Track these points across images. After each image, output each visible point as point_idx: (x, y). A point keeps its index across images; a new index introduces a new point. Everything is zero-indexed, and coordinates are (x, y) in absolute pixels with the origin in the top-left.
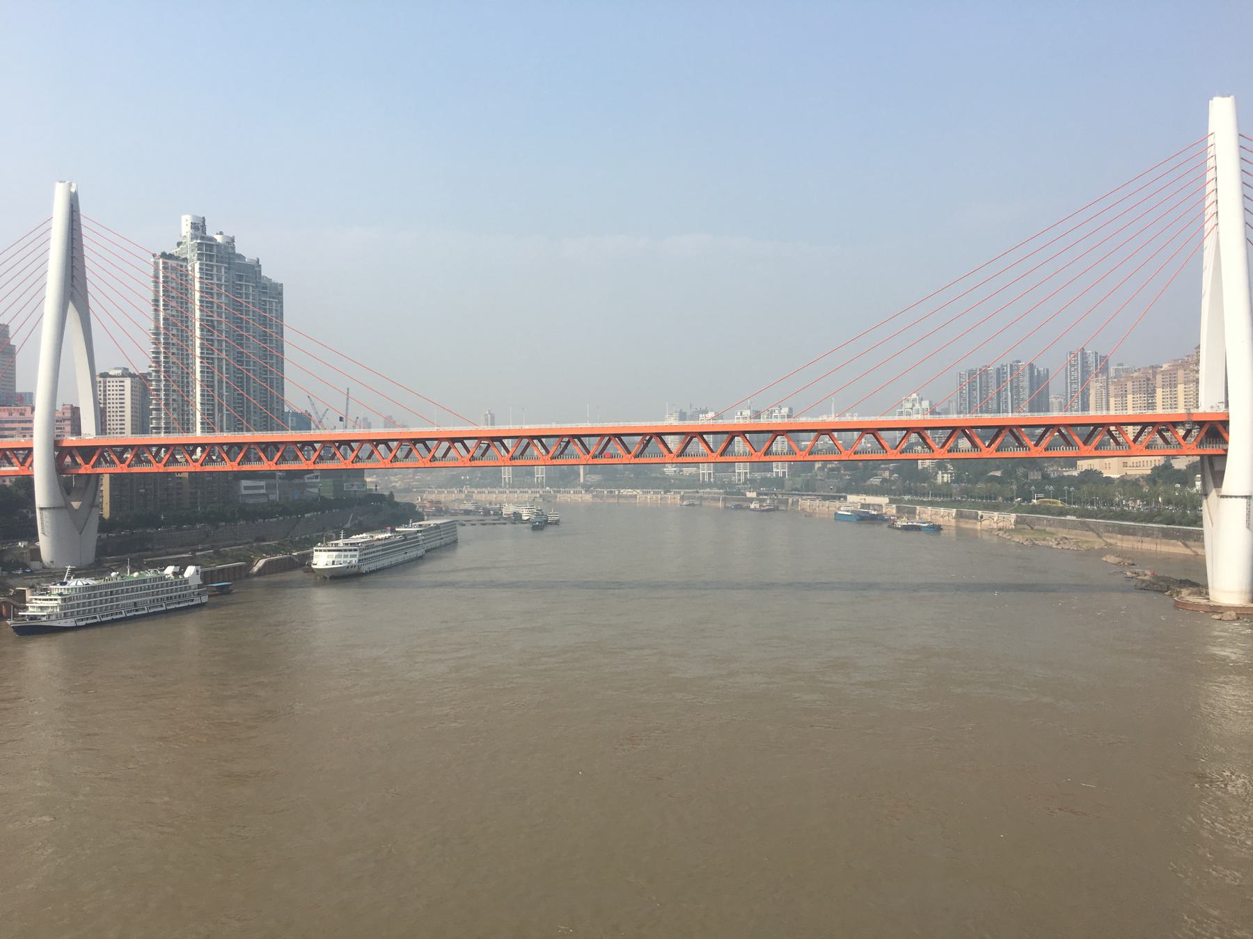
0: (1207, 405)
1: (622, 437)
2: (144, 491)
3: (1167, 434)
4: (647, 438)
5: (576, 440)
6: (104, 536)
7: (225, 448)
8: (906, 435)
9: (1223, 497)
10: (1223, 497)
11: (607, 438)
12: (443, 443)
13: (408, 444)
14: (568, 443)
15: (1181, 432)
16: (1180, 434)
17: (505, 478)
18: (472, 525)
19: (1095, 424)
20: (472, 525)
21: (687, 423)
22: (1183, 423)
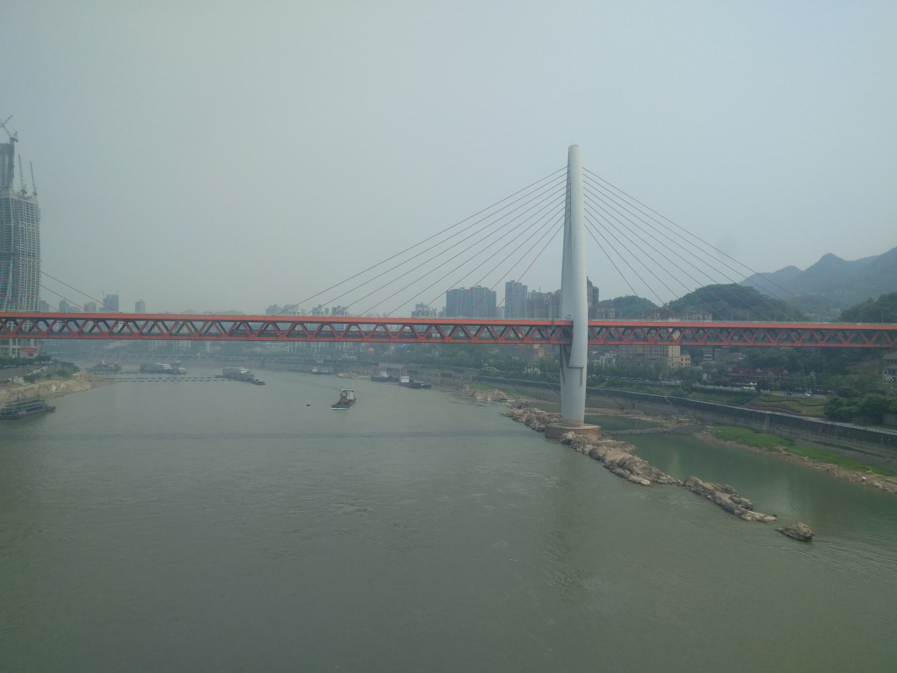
0: (563, 319)
1: (107, 321)
3: (543, 332)
4: (238, 323)
5: (217, 323)
6: (586, 414)
7: (719, 330)
8: (429, 327)
9: (570, 367)
10: (570, 367)
11: (210, 323)
12: (89, 322)
13: (61, 321)
14: (183, 325)
15: (550, 331)
16: (549, 332)
17: (151, 347)
18: (133, 381)
19: (674, 327)
20: (133, 381)
21: (511, 319)
22: (550, 326)
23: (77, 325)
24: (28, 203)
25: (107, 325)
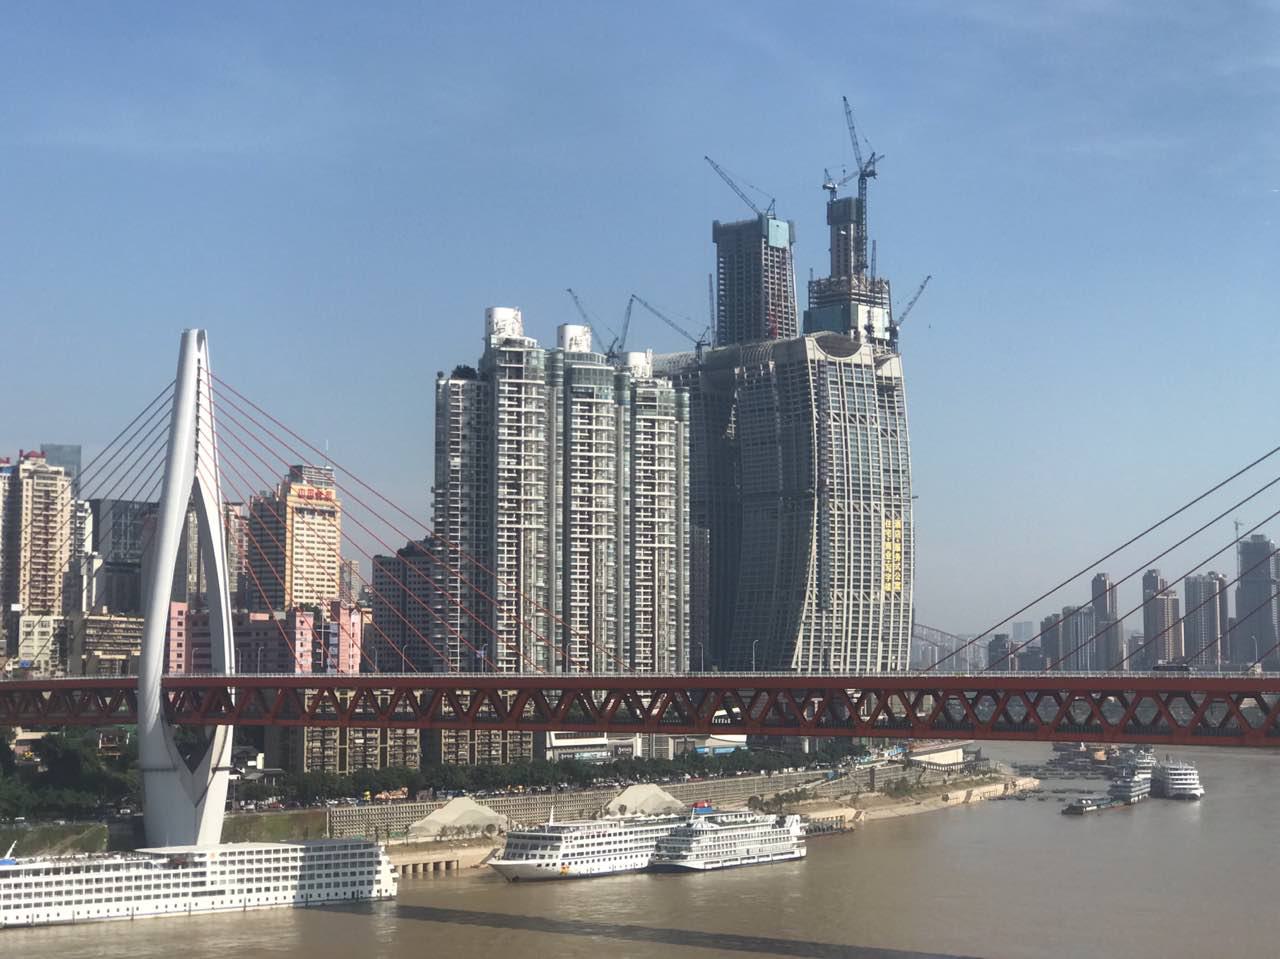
2: (362, 741)
24: (849, 365)
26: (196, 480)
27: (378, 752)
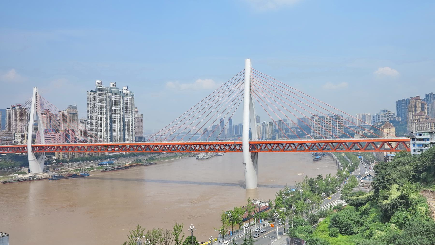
23: (282, 145)
25: (282, 145)
26: (37, 112)
27: (75, 155)
